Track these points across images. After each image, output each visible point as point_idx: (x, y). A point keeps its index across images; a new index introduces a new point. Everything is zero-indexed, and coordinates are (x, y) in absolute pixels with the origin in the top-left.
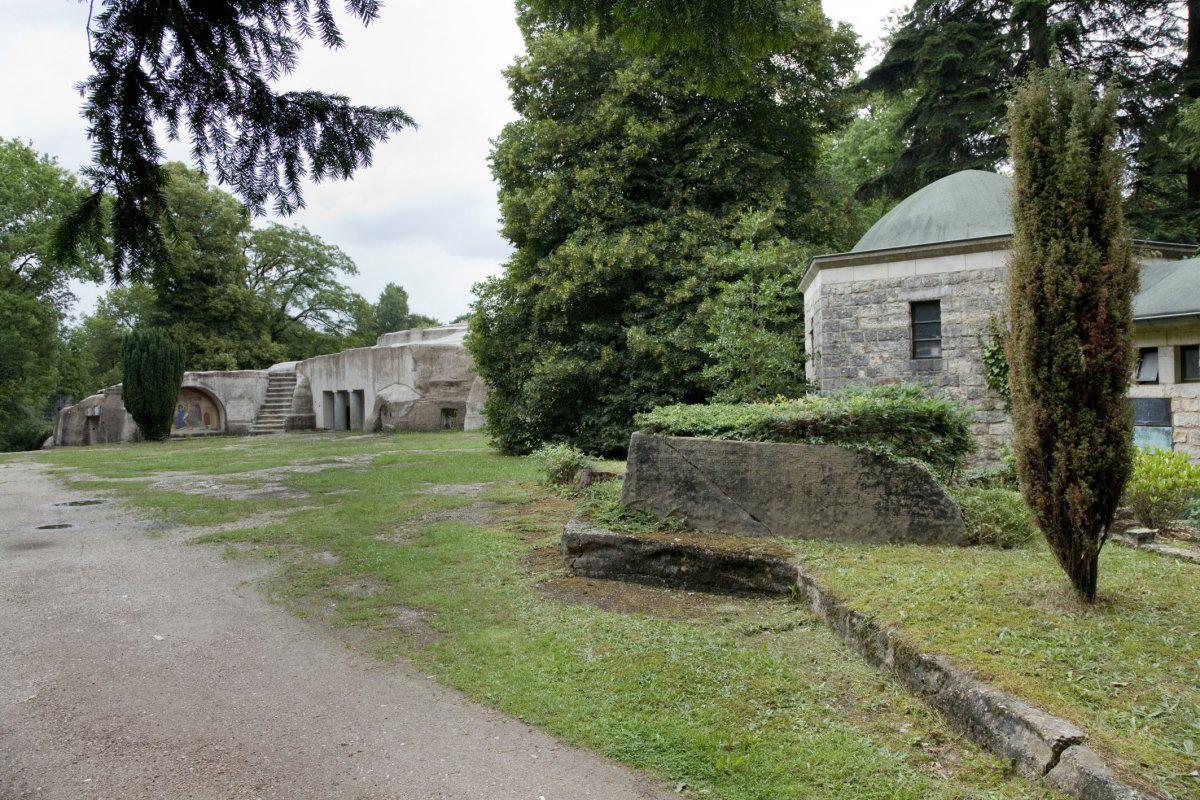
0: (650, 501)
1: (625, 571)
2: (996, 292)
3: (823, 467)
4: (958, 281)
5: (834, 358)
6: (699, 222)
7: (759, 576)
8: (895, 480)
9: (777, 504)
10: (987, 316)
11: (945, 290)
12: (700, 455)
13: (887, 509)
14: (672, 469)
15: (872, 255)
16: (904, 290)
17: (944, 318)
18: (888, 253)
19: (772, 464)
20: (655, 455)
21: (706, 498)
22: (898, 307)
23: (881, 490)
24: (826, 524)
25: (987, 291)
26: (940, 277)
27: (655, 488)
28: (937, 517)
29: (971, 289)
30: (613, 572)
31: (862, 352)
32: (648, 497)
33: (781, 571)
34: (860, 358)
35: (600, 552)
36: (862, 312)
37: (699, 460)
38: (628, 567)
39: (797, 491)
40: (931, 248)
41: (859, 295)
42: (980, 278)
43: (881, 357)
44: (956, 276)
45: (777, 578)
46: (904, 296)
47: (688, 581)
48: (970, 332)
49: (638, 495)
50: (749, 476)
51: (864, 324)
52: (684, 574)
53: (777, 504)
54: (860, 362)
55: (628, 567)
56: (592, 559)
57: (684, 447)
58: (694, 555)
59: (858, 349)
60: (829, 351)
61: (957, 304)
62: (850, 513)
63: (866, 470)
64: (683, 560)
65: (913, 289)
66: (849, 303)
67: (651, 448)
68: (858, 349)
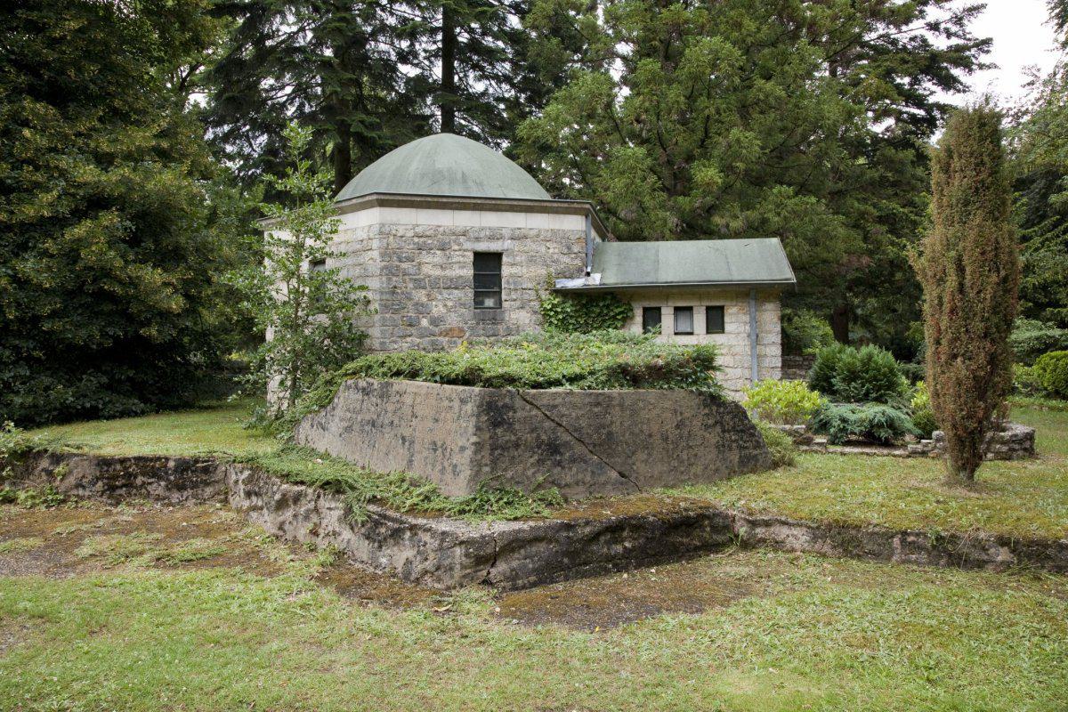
0: (509, 474)
1: (561, 567)
2: (551, 251)
3: (675, 411)
4: (519, 237)
5: (393, 304)
6: (44, 119)
7: (697, 532)
8: (727, 418)
9: (642, 456)
10: (543, 272)
11: (507, 244)
12: (564, 410)
13: (723, 446)
14: (532, 431)
15: (440, 200)
16: (469, 240)
17: (506, 271)
18: (457, 200)
19: (634, 413)
20: (511, 414)
21: (573, 460)
22: (463, 256)
23: (718, 429)
24: (683, 469)
25: (543, 249)
26: (504, 231)
27: (513, 457)
28: (755, 448)
29: (531, 246)
30: (547, 574)
31: (424, 299)
32: (505, 470)
33: (719, 521)
34: (422, 305)
35: (522, 551)
36: (426, 257)
37: (563, 416)
38: (566, 560)
39: (657, 440)
40: (499, 202)
41: (422, 240)
42: (537, 237)
43: (445, 305)
44: (518, 232)
45: (715, 529)
46: (468, 245)
47: (636, 558)
48: (530, 286)
49: (493, 469)
50: (614, 428)
51: (426, 269)
52: (631, 551)
53: (642, 456)
54: (422, 309)
55: (566, 560)
56: (515, 564)
57: (545, 402)
58: (633, 525)
59: (421, 296)
60: (388, 297)
61: (518, 259)
62: (699, 454)
63: (707, 411)
64: (625, 534)
65: (477, 239)
66: (411, 247)
67: (505, 406)
68: (421, 296)
